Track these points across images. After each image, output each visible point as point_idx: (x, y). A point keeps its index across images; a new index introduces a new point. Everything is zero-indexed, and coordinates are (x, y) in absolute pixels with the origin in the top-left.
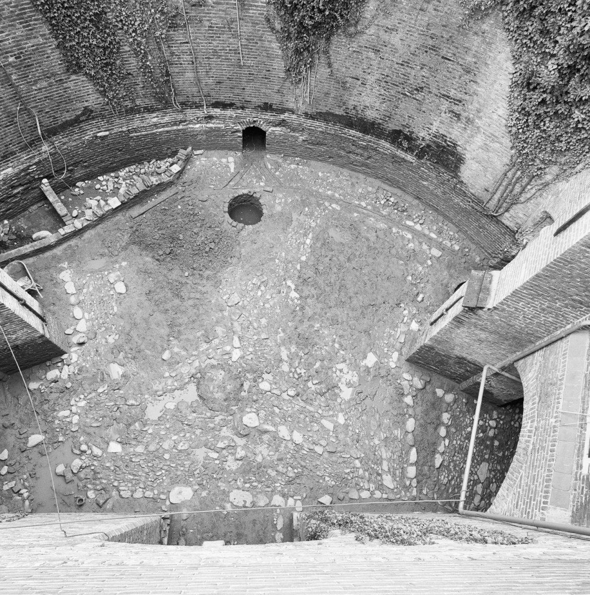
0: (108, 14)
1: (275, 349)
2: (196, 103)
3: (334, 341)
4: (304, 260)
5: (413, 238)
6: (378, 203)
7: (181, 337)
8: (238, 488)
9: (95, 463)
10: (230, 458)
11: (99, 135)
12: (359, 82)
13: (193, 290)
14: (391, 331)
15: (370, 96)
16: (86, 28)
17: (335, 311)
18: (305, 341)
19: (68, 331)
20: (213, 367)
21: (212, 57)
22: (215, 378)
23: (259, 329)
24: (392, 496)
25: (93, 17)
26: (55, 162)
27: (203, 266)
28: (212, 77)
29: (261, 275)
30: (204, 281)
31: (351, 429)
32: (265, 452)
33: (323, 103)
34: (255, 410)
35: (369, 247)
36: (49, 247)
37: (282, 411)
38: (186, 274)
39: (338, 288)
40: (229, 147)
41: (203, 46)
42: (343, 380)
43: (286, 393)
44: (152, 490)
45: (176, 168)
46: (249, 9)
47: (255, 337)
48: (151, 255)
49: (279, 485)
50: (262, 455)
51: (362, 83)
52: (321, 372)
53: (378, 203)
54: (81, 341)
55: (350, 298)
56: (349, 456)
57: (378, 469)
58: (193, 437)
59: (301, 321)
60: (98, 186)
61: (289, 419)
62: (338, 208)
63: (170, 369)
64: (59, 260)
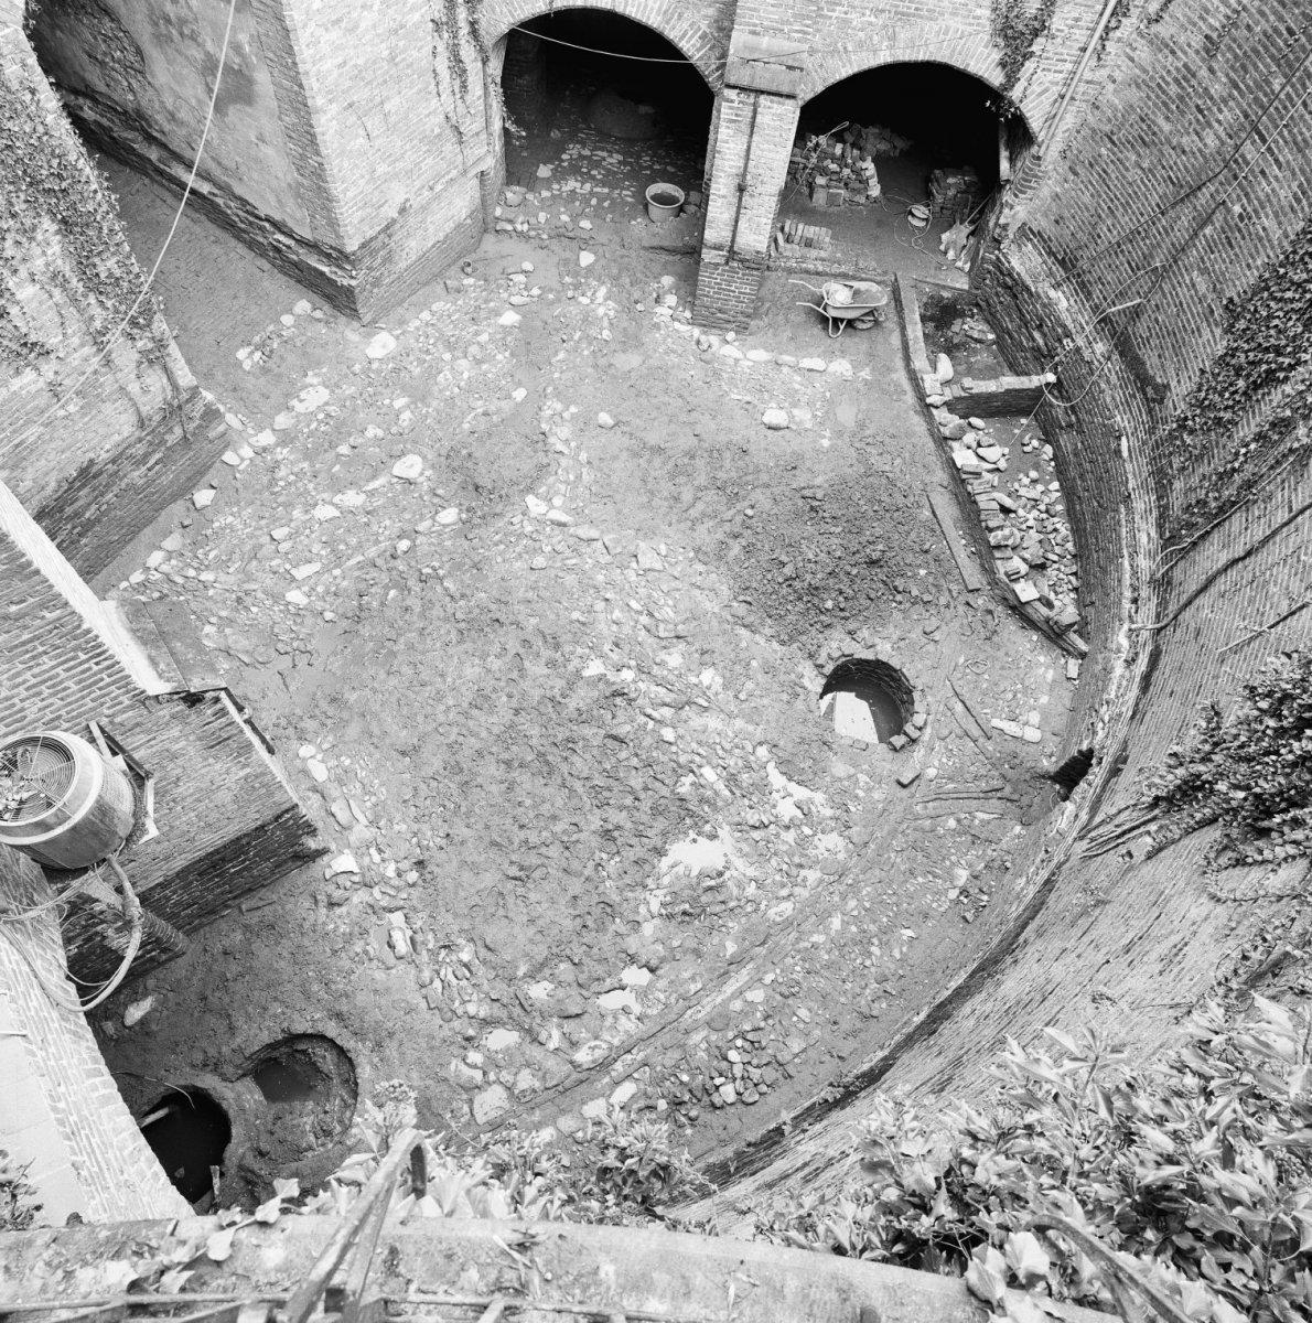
8: (327, 404)
17: (504, 715)
39: (550, 758)
55: (508, 763)
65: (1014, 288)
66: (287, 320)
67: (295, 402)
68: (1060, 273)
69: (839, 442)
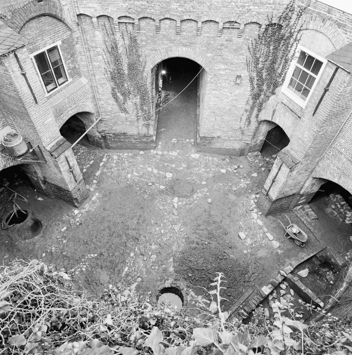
30: (195, 240)
39: (114, 234)
66: (188, 140)
69: (249, 256)
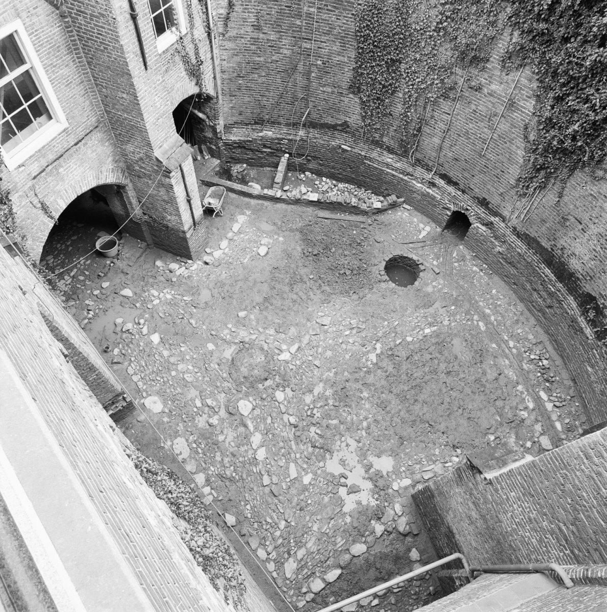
0: (402, 64)
1: (316, 380)
2: (428, 166)
3: (366, 419)
4: (409, 340)
5: (533, 410)
6: (528, 354)
7: (264, 312)
8: (187, 440)
9: (137, 336)
10: (205, 416)
11: (343, 146)
12: (580, 227)
13: (305, 291)
14: (424, 460)
15: (583, 245)
16: (380, 66)
17: (391, 397)
18: (343, 396)
19: (208, 250)
20: (262, 349)
21: (462, 135)
22: (255, 357)
23: (319, 356)
24: (280, 582)
25: (389, 61)
26: (301, 147)
27: (328, 281)
28: (453, 152)
29: (363, 322)
30: (319, 292)
31: (307, 495)
32: (230, 438)
33: (536, 228)
34: (254, 404)
35: (477, 381)
36: (250, 196)
37: (272, 425)
38: (311, 277)
39: (414, 385)
40: (433, 219)
41: (460, 124)
42: (341, 454)
43: (289, 416)
44: (144, 384)
45: (378, 205)
46: (515, 112)
47: (310, 358)
48: (303, 247)
49: (213, 470)
50: (226, 438)
51: (582, 229)
52: (331, 430)
53: (528, 354)
54: (207, 261)
56: (282, 512)
57: (293, 548)
58: (200, 378)
59: (357, 380)
60: (317, 182)
61: (270, 436)
62: (483, 328)
63: (235, 325)
64: (248, 206)
65: (241, 145)
67: (180, 458)
68: (258, 127)
